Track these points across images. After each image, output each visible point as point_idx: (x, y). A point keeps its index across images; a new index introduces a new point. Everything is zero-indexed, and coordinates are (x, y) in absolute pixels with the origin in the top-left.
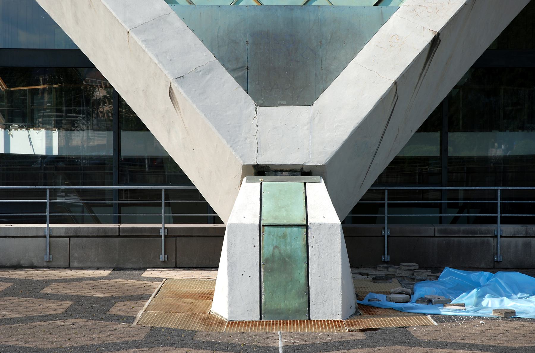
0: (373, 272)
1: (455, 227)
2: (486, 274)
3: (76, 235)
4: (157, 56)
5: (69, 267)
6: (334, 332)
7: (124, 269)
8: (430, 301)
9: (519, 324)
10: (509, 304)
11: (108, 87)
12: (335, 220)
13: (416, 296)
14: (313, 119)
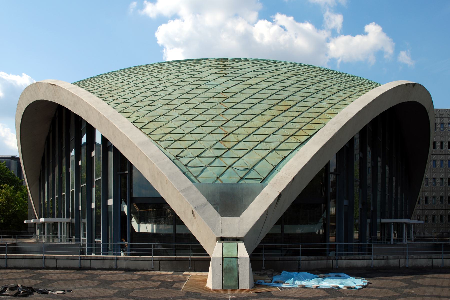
0: (259, 273)
1: (286, 257)
2: (296, 273)
3: (162, 260)
4: (188, 200)
5: (160, 271)
6: (247, 293)
7: (177, 272)
8: (278, 283)
9: (307, 290)
10: (304, 283)
11: (172, 210)
12: (246, 255)
13: (274, 281)
14: (240, 221)
